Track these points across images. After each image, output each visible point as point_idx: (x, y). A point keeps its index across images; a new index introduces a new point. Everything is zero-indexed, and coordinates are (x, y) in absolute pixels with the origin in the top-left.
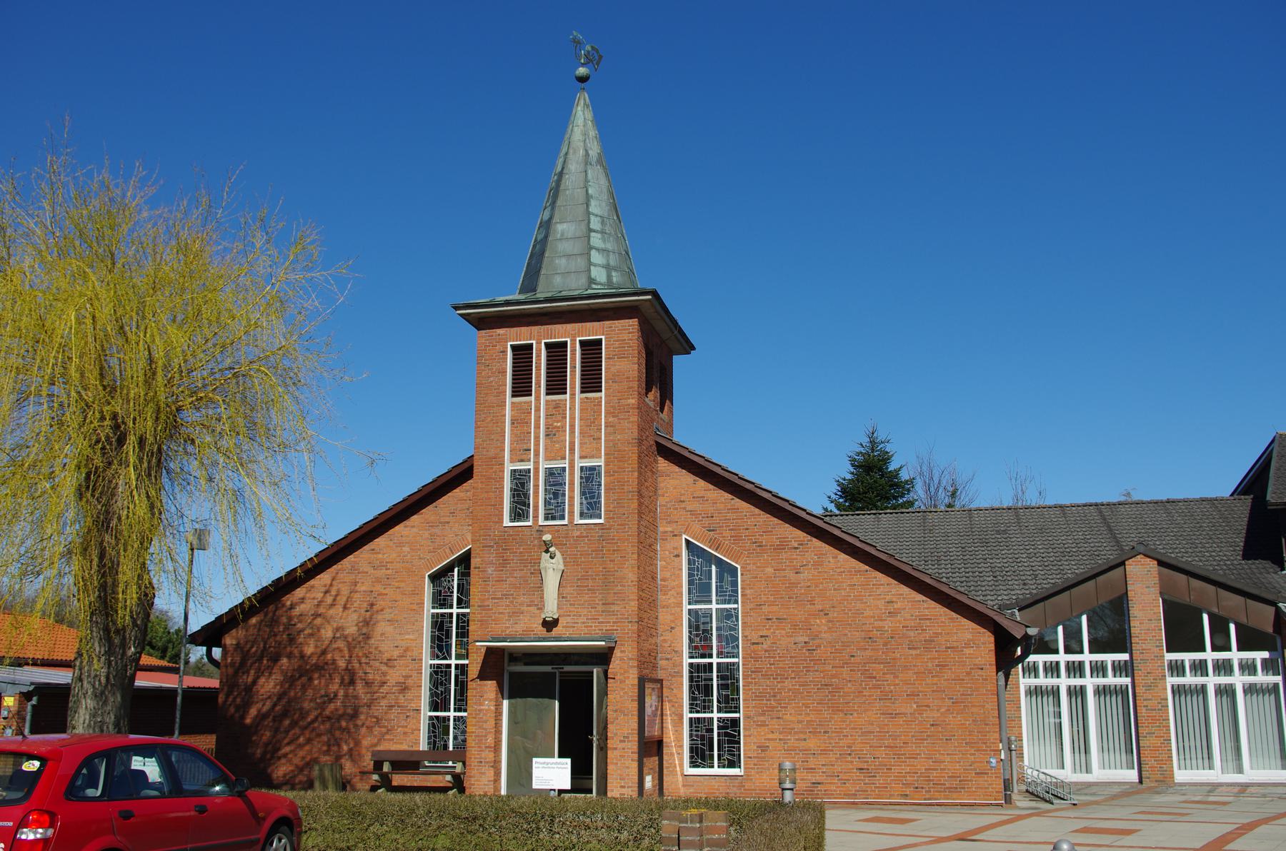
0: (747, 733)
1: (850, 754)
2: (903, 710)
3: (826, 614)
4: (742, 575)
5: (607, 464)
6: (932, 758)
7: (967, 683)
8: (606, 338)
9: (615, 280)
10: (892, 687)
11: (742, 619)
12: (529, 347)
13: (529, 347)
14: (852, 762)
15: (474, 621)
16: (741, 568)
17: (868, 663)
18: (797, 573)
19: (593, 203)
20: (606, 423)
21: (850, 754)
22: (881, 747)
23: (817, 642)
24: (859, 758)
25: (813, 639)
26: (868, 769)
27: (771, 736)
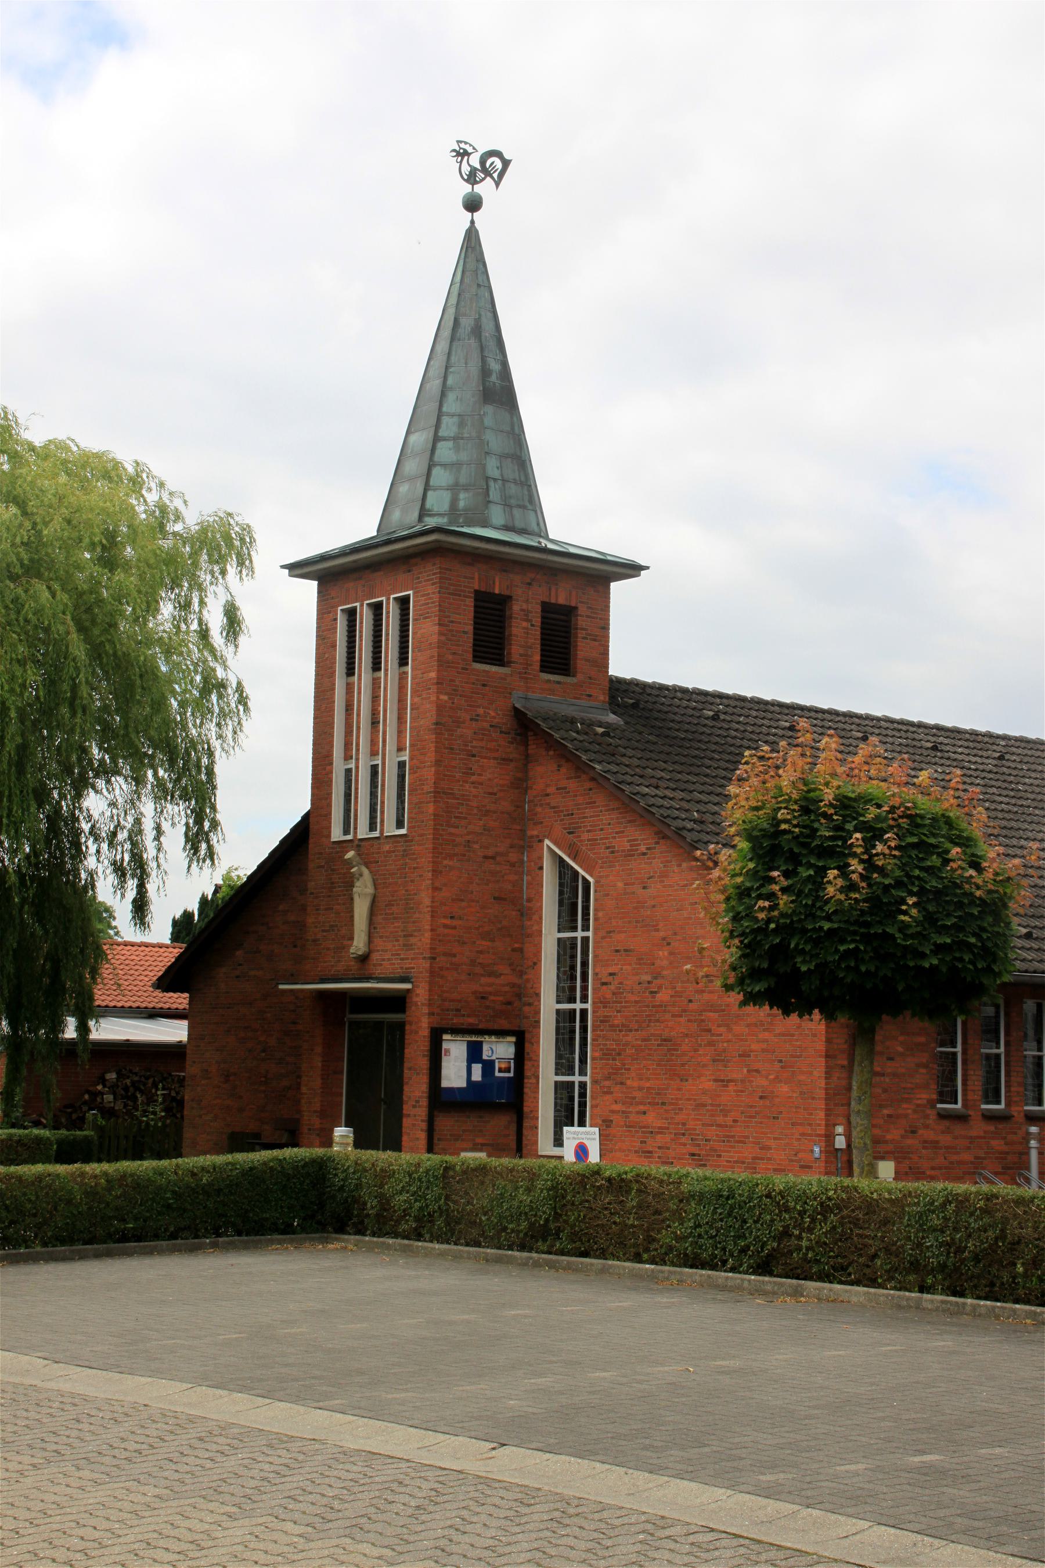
0: (594, 1102)
1: (684, 1134)
2: (734, 1076)
3: (669, 944)
4: (596, 891)
5: (411, 759)
6: (759, 1143)
7: (797, 1040)
8: (414, 593)
9: (462, 504)
10: (725, 1044)
11: (594, 952)
12: (504, 601)
13: (504, 601)
14: (685, 1145)
15: (819, 1099)
16: (596, 882)
17: (705, 1011)
18: (644, 888)
19: (451, 396)
20: (412, 705)
21: (684, 1134)
22: (712, 1125)
23: (659, 981)
24: (692, 1140)
25: (656, 978)
26: (699, 1155)
27: (615, 1107)
